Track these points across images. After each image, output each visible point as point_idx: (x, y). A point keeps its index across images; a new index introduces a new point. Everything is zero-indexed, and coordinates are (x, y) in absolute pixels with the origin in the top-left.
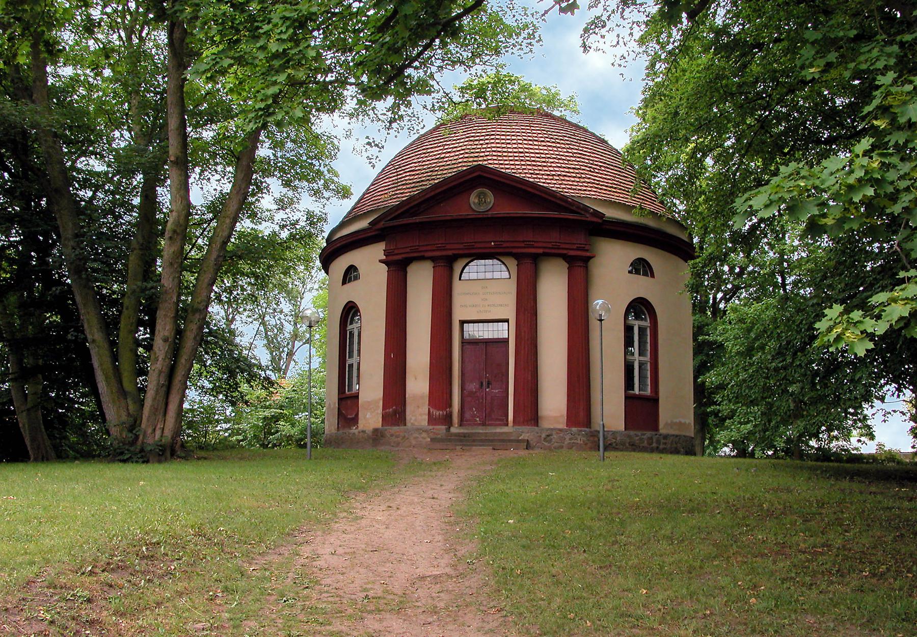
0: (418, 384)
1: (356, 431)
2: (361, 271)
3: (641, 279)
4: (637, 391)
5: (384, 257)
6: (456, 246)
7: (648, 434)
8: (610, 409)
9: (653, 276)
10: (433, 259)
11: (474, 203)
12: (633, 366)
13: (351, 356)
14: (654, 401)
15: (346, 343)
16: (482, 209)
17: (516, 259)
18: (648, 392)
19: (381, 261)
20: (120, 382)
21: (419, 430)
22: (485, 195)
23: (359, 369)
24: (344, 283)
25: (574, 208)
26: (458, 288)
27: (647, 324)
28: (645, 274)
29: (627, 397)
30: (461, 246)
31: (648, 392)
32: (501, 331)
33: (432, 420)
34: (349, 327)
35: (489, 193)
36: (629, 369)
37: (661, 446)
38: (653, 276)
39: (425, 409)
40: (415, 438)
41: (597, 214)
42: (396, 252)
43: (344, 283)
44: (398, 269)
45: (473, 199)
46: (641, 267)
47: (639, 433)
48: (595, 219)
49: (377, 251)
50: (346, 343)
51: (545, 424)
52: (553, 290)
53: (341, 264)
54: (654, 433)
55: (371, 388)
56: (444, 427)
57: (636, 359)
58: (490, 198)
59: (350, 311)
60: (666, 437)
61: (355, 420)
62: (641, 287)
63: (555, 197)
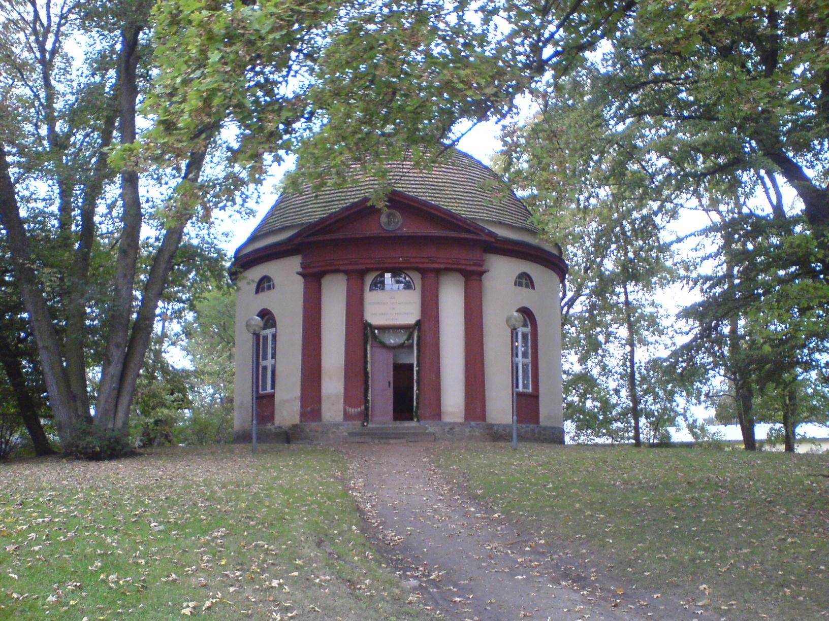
0: (333, 385)
1: (272, 427)
3: (524, 291)
4: (521, 389)
7: (532, 426)
8: (500, 407)
9: (533, 288)
10: (346, 272)
13: (265, 358)
15: (261, 346)
16: (392, 228)
17: (464, 276)
18: (530, 390)
20: (68, 386)
24: (257, 292)
25: (471, 229)
28: (527, 286)
31: (530, 390)
33: (347, 416)
35: (398, 214)
37: (542, 437)
38: (533, 288)
39: (341, 405)
41: (491, 234)
43: (257, 292)
44: (313, 279)
46: (525, 280)
47: (524, 426)
48: (488, 238)
49: (294, 264)
50: (261, 346)
51: (447, 419)
52: (452, 300)
60: (545, 428)
61: (271, 418)
62: (525, 298)
63: (456, 219)
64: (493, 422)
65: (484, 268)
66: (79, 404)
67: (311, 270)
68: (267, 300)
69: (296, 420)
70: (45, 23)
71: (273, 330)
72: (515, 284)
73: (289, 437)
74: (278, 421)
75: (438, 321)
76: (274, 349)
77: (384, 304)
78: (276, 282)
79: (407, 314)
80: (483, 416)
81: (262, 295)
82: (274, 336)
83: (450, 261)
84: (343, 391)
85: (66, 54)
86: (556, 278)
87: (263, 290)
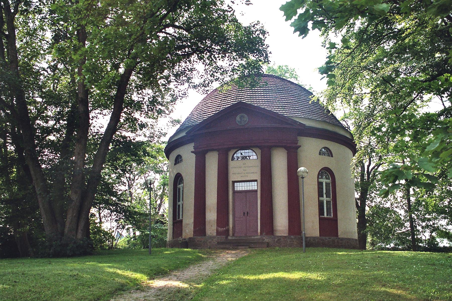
0: (211, 215)
2: (183, 158)
5: (194, 150)
7: (333, 238)
8: (311, 226)
9: (332, 156)
11: (238, 121)
12: (323, 203)
13: (179, 201)
14: (335, 220)
19: (192, 152)
21: (212, 237)
22: (243, 117)
23: (182, 207)
26: (232, 164)
29: (320, 219)
32: (254, 186)
33: (218, 233)
34: (178, 186)
36: (321, 204)
38: (332, 156)
39: (215, 227)
40: (210, 242)
43: (175, 164)
45: (238, 118)
47: (327, 238)
48: (300, 128)
49: (190, 147)
52: (280, 162)
54: (335, 238)
55: (188, 220)
56: (224, 236)
57: (325, 199)
58: (246, 118)
60: (342, 239)
61: (181, 234)
62: (326, 162)
66: (59, 225)
71: (182, 185)
72: (320, 154)
74: (183, 237)
78: (183, 158)
81: (177, 165)
84: (287, 228)
85: (325, 155)
86: (351, 153)
87: (178, 163)
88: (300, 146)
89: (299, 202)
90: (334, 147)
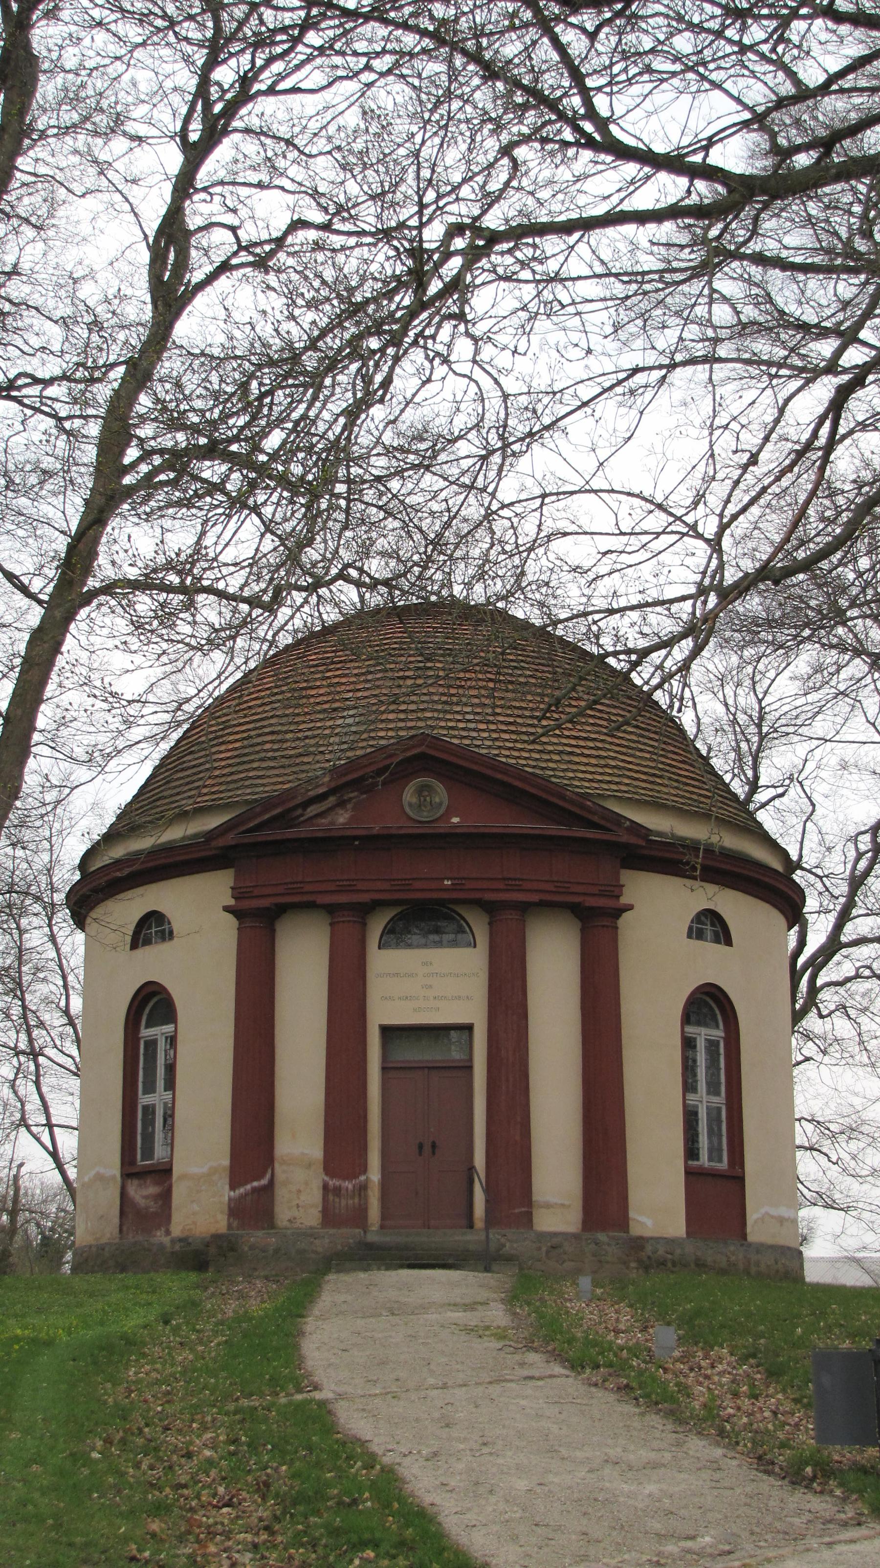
1: (166, 1240)
3: (711, 950)
5: (232, 902)
6: (379, 885)
9: (729, 942)
10: (331, 910)
11: (410, 805)
13: (150, 1088)
14: (735, 1179)
16: (425, 816)
24: (134, 946)
25: (596, 819)
27: (718, 1033)
28: (717, 941)
29: (691, 1174)
30: (386, 886)
33: (329, 1217)
36: (690, 1117)
38: (729, 942)
41: (636, 828)
42: (256, 892)
43: (134, 946)
44: (259, 924)
45: (409, 796)
46: (711, 927)
48: (633, 840)
52: (553, 962)
53: (127, 909)
57: (703, 1100)
58: (441, 794)
59: (151, 1004)
60: (761, 1248)
62: (710, 964)
64: (647, 1234)
65: (624, 900)
67: (247, 904)
68: (155, 964)
69: (219, 1223)
70: (323, 26)
71: (169, 1028)
72: (689, 936)
73: (199, 1258)
74: (177, 1228)
75: (524, 1015)
76: (171, 1069)
77: (411, 975)
79: (459, 998)
80: (622, 1221)
81: (140, 952)
82: (172, 1040)
83: (550, 887)
87: (147, 942)
88: (630, 908)
89: (489, 1084)
90: (734, 906)
